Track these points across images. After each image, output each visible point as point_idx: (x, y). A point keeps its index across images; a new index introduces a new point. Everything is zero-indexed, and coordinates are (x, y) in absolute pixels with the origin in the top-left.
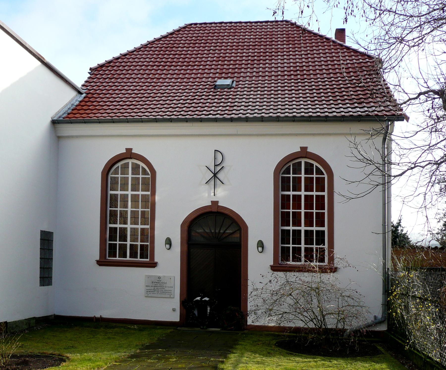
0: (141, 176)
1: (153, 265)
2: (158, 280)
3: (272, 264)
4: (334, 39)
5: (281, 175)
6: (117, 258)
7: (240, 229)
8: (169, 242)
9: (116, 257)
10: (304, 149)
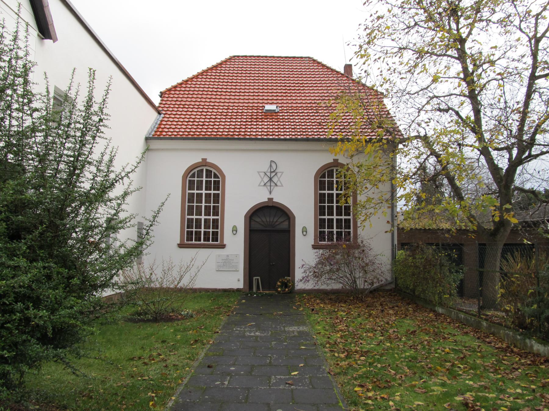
0: (213, 179)
3: (313, 243)
4: (343, 72)
6: (194, 242)
10: (204, 160)
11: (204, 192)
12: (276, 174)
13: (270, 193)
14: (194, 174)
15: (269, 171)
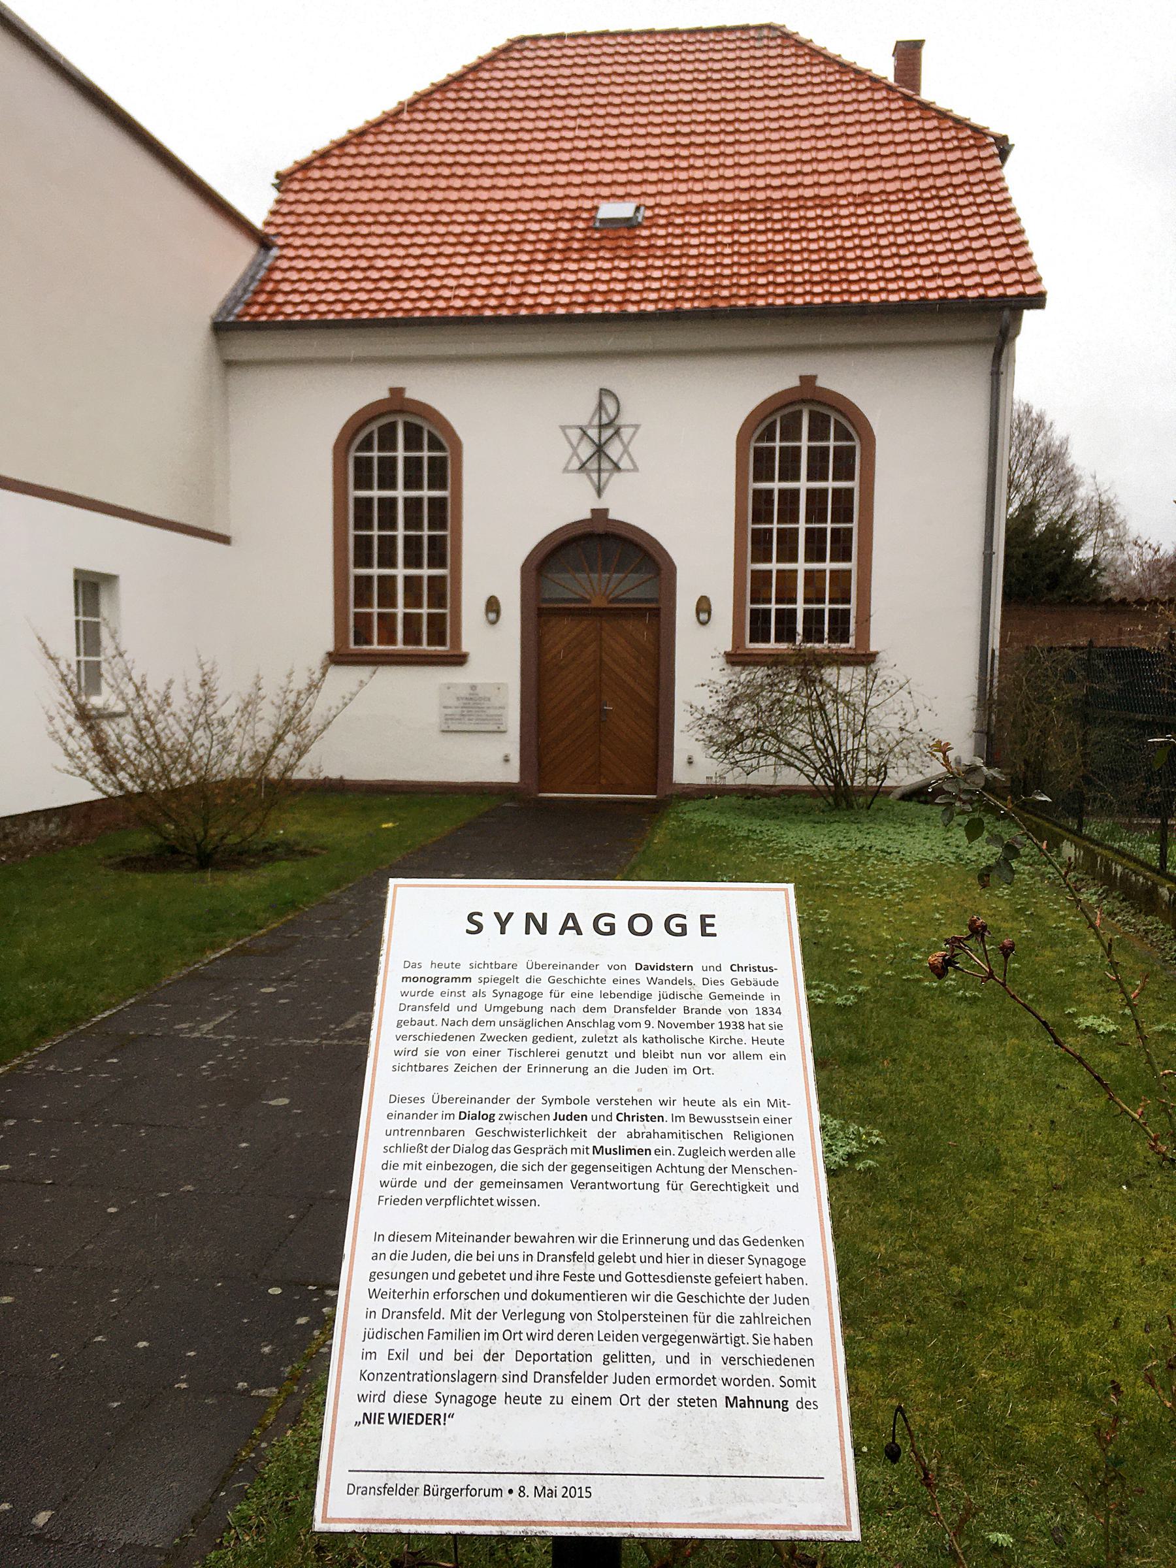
0: (426, 454)
1: (458, 659)
4: (891, 80)
5: (753, 444)
8: (493, 606)
10: (397, 392)
11: (400, 493)
12: (617, 432)
13: (599, 491)
14: (369, 438)
15: (596, 422)
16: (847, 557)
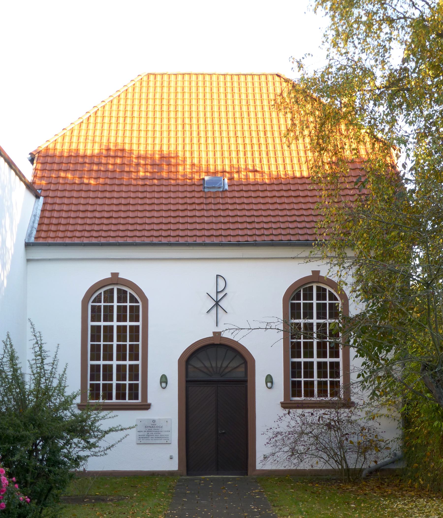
0: (128, 304)
1: (146, 407)
2: (153, 423)
3: (283, 400)
7: (245, 362)
8: (164, 380)
9: (125, 400)
10: (115, 275)
16: (337, 356)
